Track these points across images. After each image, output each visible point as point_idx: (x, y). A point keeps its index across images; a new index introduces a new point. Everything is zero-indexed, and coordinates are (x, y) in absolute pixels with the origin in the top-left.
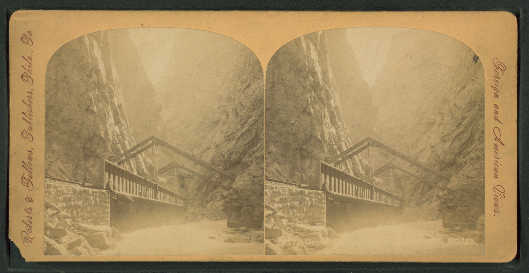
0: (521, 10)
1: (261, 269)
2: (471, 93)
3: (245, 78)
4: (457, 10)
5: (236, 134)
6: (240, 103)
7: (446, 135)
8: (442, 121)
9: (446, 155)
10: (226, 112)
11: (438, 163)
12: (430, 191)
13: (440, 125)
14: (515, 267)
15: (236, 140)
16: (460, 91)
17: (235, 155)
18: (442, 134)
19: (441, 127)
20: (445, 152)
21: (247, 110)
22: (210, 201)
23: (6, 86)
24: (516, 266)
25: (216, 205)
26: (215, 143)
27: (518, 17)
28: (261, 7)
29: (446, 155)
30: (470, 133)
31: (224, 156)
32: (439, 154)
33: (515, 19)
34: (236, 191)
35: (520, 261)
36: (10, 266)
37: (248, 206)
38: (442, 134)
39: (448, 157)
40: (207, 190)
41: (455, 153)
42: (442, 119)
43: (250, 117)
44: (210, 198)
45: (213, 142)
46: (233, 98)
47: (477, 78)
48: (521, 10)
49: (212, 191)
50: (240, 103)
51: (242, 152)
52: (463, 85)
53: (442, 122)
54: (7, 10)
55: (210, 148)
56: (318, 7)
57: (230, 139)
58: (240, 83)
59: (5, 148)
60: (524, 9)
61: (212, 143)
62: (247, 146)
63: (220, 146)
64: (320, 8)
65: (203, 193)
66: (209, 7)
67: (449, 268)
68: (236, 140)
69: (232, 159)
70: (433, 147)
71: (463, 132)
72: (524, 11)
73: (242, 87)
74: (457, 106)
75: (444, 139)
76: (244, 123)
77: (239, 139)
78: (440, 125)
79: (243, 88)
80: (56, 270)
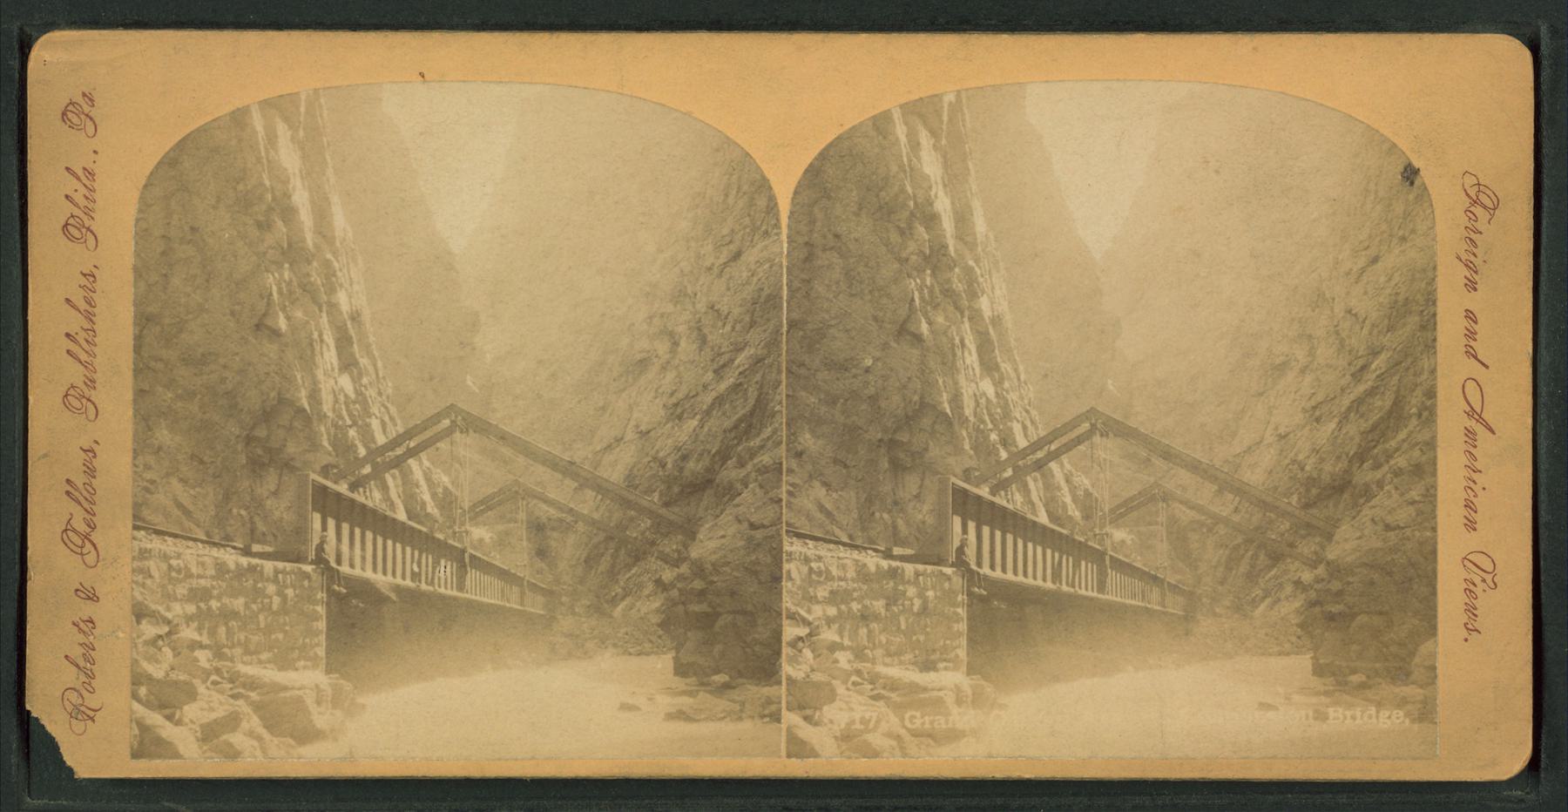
0: (1544, 30)
1: (773, 801)
2: (1396, 278)
3: (725, 231)
4: (1356, 30)
5: (699, 399)
6: (712, 307)
7: (1322, 403)
8: (1310, 359)
9: (1322, 460)
10: (671, 334)
11: (1298, 485)
12: (1276, 569)
13: (1303, 371)
14: (1527, 793)
15: (698, 417)
16: (1363, 270)
17: (698, 461)
18: (1310, 399)
19: (1308, 379)
20: (1318, 452)
21: (733, 328)
22: (623, 599)
23: (19, 256)
24: (1528, 790)
25: (639, 610)
26: (637, 426)
27: (1535, 49)
28: (773, 20)
29: (1322, 460)
30: (1393, 396)
31: (663, 466)
32: (1301, 457)
33: (1527, 55)
34: (699, 570)
35: (1542, 775)
36: (29, 792)
37: (734, 612)
38: (1310, 399)
39: (1328, 467)
40: (613, 566)
41: (709, 452)
42: (1311, 353)
43: (742, 349)
44: (624, 589)
45: (632, 423)
46: (689, 291)
47: (1413, 231)
48: (1544, 30)
49: (629, 567)
50: (712, 307)
51: (718, 452)
52: (1373, 252)
53: (1311, 362)
54: (21, 29)
55: (622, 439)
56: (941, 20)
57: (682, 413)
58: (710, 247)
59: (15, 442)
60: (1552, 26)
61: (629, 427)
62: (733, 435)
63: (652, 433)
64: (947, 23)
65: (602, 573)
66: (621, 22)
67: (1331, 796)
68: (698, 417)
69: (687, 473)
70: (1282, 437)
71: (1371, 392)
72: (1554, 32)
73: (718, 258)
74: (1356, 315)
75: (1317, 413)
76: (724, 366)
77: (708, 413)
78: (1303, 371)
79: (722, 261)
80: (166, 804)
